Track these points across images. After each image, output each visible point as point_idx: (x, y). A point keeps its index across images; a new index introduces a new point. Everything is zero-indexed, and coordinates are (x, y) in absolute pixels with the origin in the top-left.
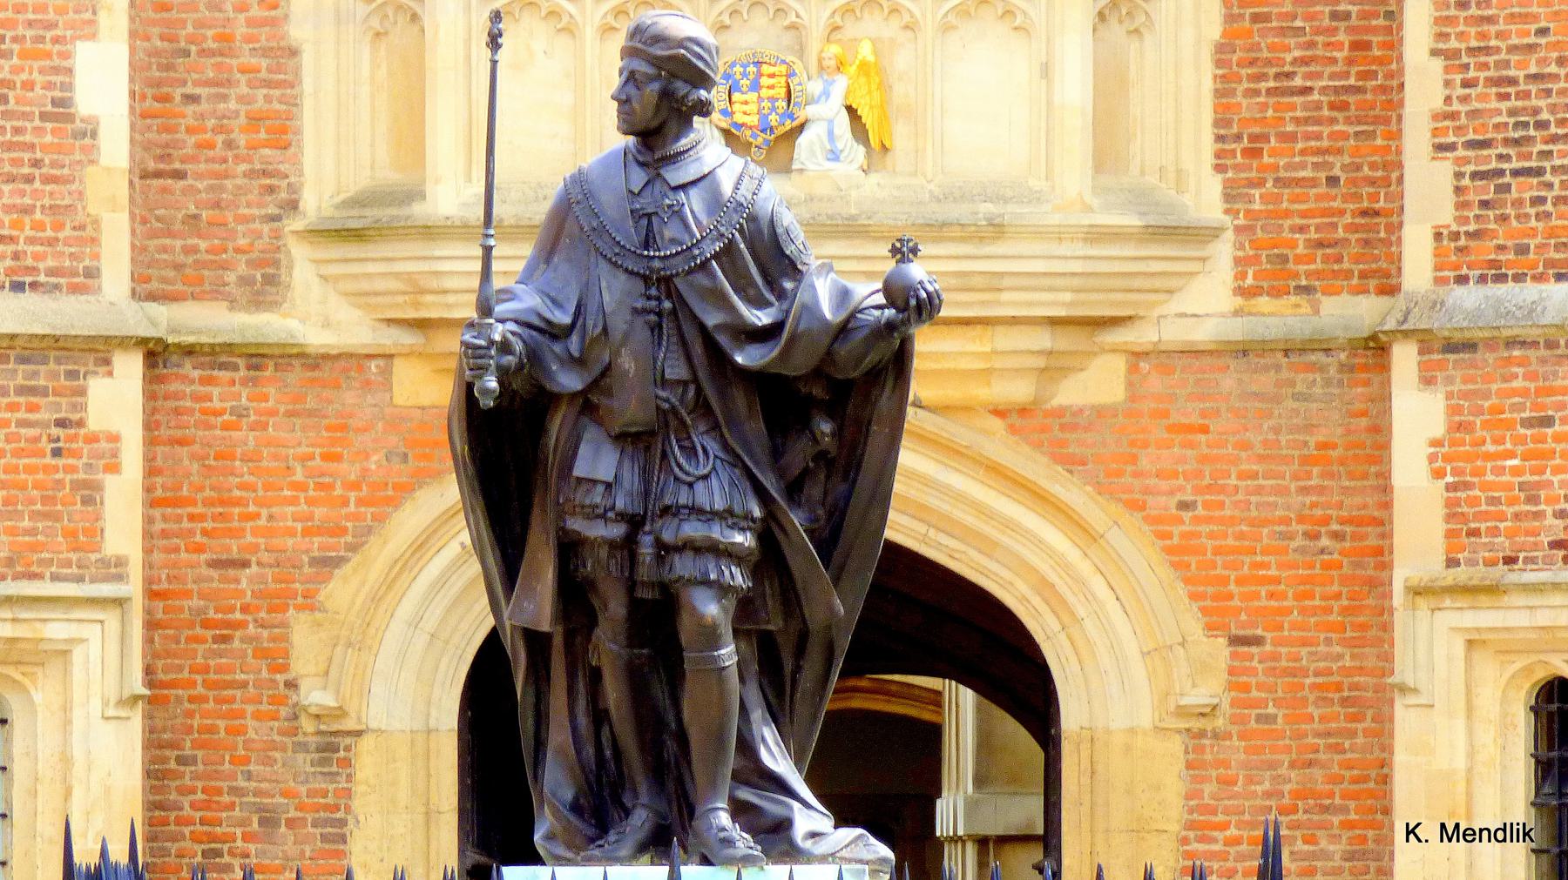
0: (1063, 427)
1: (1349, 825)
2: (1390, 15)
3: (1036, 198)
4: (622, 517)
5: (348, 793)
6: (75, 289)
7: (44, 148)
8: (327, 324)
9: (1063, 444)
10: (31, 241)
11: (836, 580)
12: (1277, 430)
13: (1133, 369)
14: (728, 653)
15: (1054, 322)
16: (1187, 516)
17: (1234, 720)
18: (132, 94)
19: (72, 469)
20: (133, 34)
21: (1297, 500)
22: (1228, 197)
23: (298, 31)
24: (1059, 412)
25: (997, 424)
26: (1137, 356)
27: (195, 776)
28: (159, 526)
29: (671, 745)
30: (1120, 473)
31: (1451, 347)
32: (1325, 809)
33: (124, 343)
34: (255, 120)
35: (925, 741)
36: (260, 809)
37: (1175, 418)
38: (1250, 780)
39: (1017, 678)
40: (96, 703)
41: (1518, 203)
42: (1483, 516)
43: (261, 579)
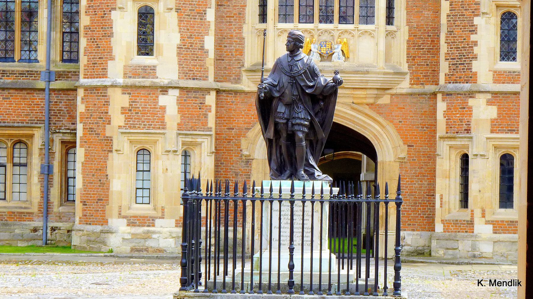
0: (379, 107)
1: (428, 179)
2: (438, 36)
3: (375, 67)
4: (286, 119)
5: (251, 170)
6: (204, 80)
7: (199, 55)
8: (249, 87)
9: (379, 110)
10: (196, 71)
11: (323, 131)
12: (417, 109)
13: (391, 97)
14: (304, 143)
15: (377, 89)
16: (400, 123)
17: (408, 160)
18: (215, 45)
19: (203, 112)
20: (215, 35)
21: (420, 121)
22: (409, 67)
23: (244, 35)
24: (378, 105)
25: (367, 107)
26: (392, 95)
27: (224, 166)
28: (218, 122)
29: (294, 159)
30: (389, 116)
31: (447, 95)
32: (424, 176)
33: (212, 89)
34: (237, 50)
35: (359, 164)
36: (235, 172)
37: (399, 106)
38: (411, 171)
39: (372, 154)
40: (206, 153)
41: (460, 69)
42: (453, 125)
43: (236, 132)
